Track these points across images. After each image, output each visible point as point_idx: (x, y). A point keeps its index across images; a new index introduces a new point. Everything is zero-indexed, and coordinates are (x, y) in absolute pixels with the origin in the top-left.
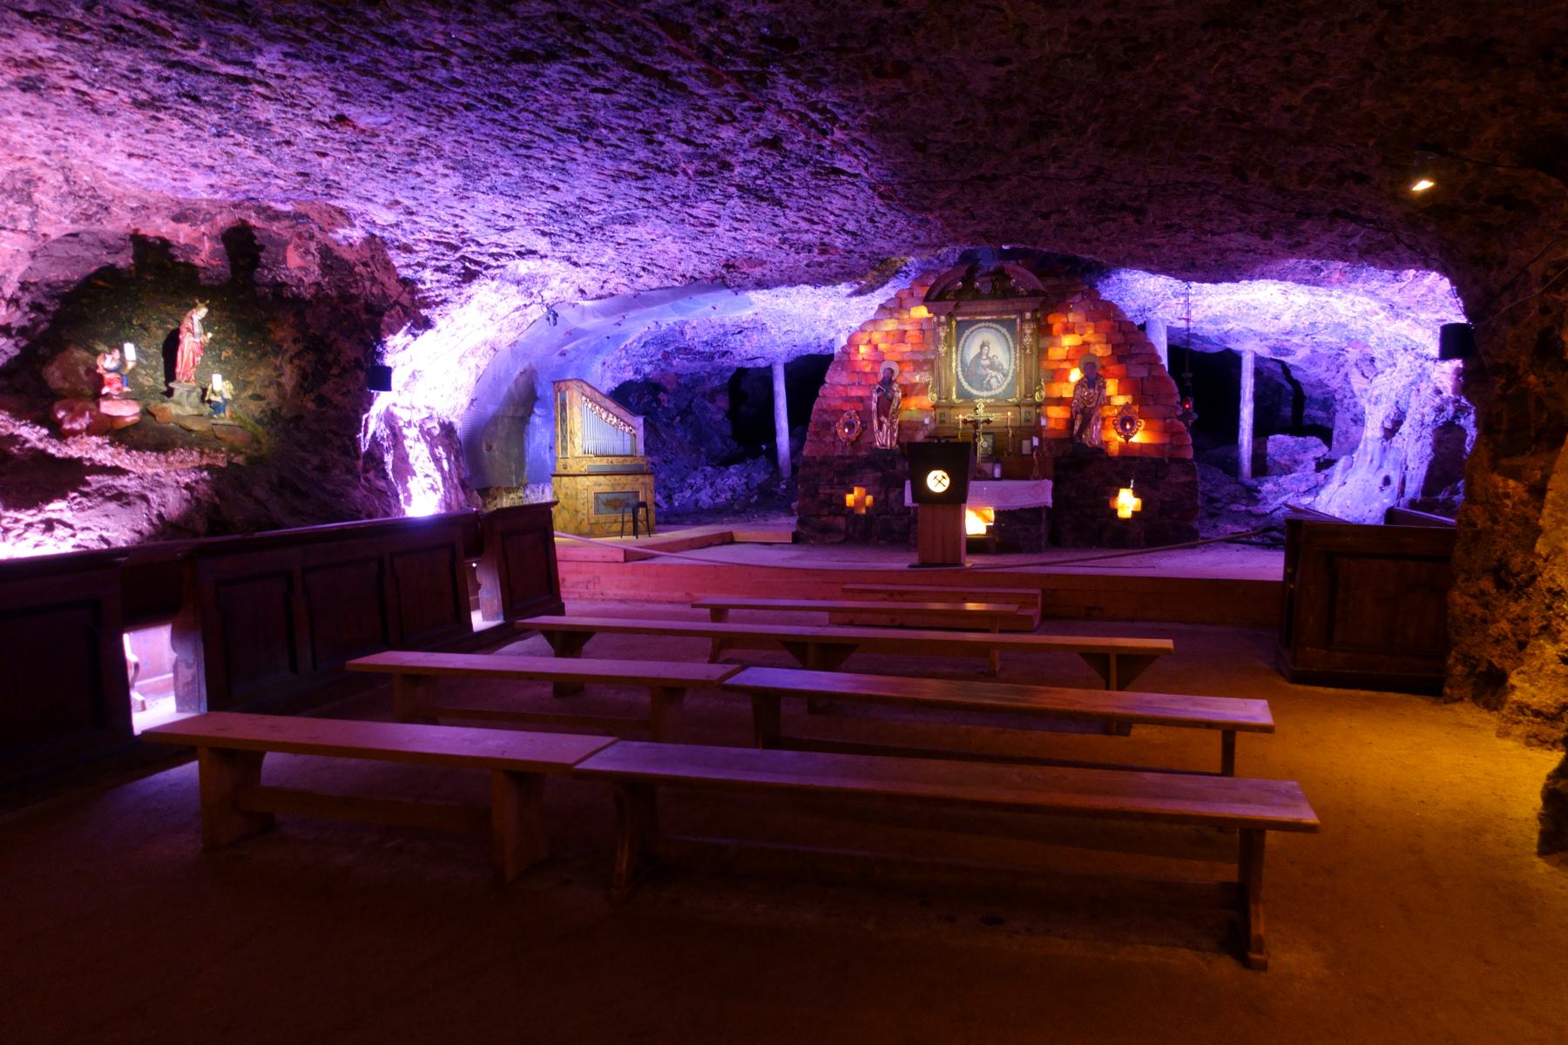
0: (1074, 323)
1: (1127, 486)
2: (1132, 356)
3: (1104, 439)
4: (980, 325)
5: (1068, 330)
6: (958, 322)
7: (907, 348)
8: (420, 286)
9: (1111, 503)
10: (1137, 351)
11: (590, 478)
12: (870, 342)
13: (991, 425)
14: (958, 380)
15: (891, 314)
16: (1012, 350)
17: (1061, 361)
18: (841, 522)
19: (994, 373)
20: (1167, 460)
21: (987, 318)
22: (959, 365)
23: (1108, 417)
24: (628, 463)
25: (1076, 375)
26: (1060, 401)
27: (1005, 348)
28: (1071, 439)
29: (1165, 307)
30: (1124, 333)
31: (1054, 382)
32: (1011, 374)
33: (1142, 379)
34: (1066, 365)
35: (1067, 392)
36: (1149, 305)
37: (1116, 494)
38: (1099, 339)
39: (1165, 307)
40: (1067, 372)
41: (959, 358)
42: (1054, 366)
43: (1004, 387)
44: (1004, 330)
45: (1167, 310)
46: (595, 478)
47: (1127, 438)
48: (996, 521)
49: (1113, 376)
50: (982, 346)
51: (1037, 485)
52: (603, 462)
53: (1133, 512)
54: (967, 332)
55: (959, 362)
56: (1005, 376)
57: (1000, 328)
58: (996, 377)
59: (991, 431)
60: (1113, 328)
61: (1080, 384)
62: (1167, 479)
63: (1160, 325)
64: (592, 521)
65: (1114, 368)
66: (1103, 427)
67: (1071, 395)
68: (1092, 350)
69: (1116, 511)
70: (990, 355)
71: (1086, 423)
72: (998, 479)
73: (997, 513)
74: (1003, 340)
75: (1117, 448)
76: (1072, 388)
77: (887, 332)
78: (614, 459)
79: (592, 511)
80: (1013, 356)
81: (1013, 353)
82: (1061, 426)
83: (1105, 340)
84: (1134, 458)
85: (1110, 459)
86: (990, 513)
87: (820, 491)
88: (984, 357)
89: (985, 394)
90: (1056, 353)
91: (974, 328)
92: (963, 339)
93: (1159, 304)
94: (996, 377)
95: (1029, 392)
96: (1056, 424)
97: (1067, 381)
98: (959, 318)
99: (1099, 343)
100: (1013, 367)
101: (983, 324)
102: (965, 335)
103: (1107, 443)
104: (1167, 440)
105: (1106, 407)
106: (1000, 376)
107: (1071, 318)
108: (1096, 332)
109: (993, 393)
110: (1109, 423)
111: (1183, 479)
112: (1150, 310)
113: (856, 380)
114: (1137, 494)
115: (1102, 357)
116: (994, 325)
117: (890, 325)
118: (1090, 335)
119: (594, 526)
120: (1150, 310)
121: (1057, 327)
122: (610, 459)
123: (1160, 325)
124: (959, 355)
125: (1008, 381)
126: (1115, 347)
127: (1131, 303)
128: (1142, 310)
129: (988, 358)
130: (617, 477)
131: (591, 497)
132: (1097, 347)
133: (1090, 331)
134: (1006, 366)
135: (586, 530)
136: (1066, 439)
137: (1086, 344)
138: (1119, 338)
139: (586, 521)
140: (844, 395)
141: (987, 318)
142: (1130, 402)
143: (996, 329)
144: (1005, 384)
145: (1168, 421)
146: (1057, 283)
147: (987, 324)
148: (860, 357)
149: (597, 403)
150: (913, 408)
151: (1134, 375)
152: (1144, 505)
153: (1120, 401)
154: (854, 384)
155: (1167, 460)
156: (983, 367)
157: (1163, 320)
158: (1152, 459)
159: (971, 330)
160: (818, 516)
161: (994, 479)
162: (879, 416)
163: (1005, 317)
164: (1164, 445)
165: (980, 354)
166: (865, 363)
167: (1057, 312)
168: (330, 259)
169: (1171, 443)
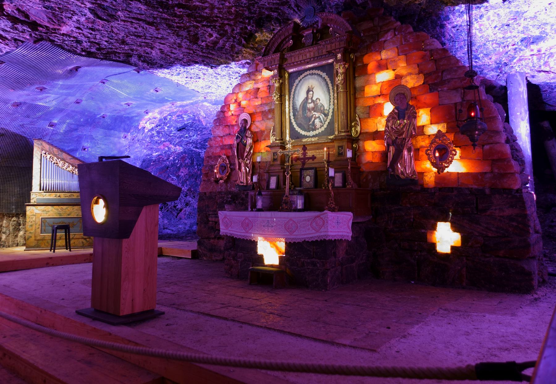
0: (387, 59)
1: (445, 220)
2: (443, 83)
3: (418, 169)
4: (306, 73)
5: (381, 66)
6: (290, 74)
7: (258, 102)
8: (307, 154)
9: (428, 237)
10: (449, 77)
11: (39, 207)
12: (236, 101)
13: (315, 161)
14: (291, 123)
15: (249, 77)
16: (331, 91)
17: (375, 97)
18: (222, 243)
19: (317, 115)
20: (487, 191)
21: (310, 66)
22: (291, 111)
23: (422, 147)
24: (75, 197)
25: (388, 108)
26: (376, 135)
27: (325, 89)
28: (387, 171)
29: (520, 60)
30: (435, 61)
31: (369, 117)
32: (330, 114)
33: (456, 104)
34: (380, 101)
35: (380, 125)
36: (504, 60)
37: (434, 228)
38: (410, 71)
39: (520, 60)
40: (381, 106)
41: (291, 105)
42: (370, 103)
43: (325, 126)
44: (324, 75)
45: (524, 63)
46: (43, 207)
47: (441, 169)
48: (286, 252)
49: (424, 106)
50: (308, 92)
51: (318, 216)
52: (52, 197)
53: (453, 248)
54: (297, 81)
55: (291, 108)
56: (326, 115)
57: (321, 73)
58: (319, 117)
59: (313, 166)
60: (423, 57)
61: (392, 116)
62: (488, 213)
63: (519, 78)
64: (38, 238)
65: (427, 98)
66: (417, 158)
67: (383, 129)
68: (403, 82)
69: (434, 245)
70: (314, 99)
71: (398, 155)
72: (300, 210)
73: (288, 245)
74: (323, 84)
75: (433, 179)
76: (383, 121)
77: (247, 92)
78: (62, 194)
79: (39, 230)
80: (332, 97)
81: (332, 94)
82: (376, 160)
83: (417, 70)
84: (451, 189)
85: (424, 190)
86: (282, 245)
87: (210, 219)
88: (310, 101)
89: (311, 133)
90: (372, 90)
91: (301, 77)
92: (294, 87)
93: (514, 58)
94: (319, 117)
95: (348, 128)
96: (373, 158)
97: (381, 115)
98: (291, 70)
99: (410, 74)
100: (332, 107)
101: (308, 72)
102: (295, 84)
103: (422, 174)
104: (487, 169)
105: (420, 138)
106: (322, 116)
107: (384, 55)
108: (408, 62)
109: (317, 132)
110: (422, 153)
111: (508, 212)
112: (506, 64)
113: (228, 132)
114: (455, 228)
115: (414, 88)
116: (316, 72)
117: (249, 86)
118: (402, 68)
119: (40, 242)
120: (506, 64)
121: (371, 66)
122: (58, 194)
123: (519, 78)
124: (291, 102)
125: (328, 121)
126: (427, 76)
127: (486, 60)
128: (499, 66)
129: (313, 101)
130: (64, 207)
131: (39, 221)
132: (408, 78)
133: (403, 64)
134: (326, 107)
135: (33, 244)
136: (382, 172)
137: (398, 77)
138: (431, 66)
139: (33, 238)
140: (221, 144)
141: (310, 66)
142: (444, 130)
143: (318, 75)
144: (327, 123)
145: (487, 147)
146: (370, 25)
147: (311, 72)
148: (230, 113)
149: (55, 155)
150: (263, 151)
151: (446, 102)
152: (463, 240)
153: (433, 130)
154: (227, 135)
155: (487, 191)
156: (309, 110)
157: (521, 74)
158: (470, 190)
159: (299, 78)
160: (209, 238)
161: (296, 210)
162: (238, 159)
163: (324, 62)
164: (483, 174)
165: (307, 98)
166: (233, 117)
167: (371, 52)
168: (414, 172)
169: (492, 172)
